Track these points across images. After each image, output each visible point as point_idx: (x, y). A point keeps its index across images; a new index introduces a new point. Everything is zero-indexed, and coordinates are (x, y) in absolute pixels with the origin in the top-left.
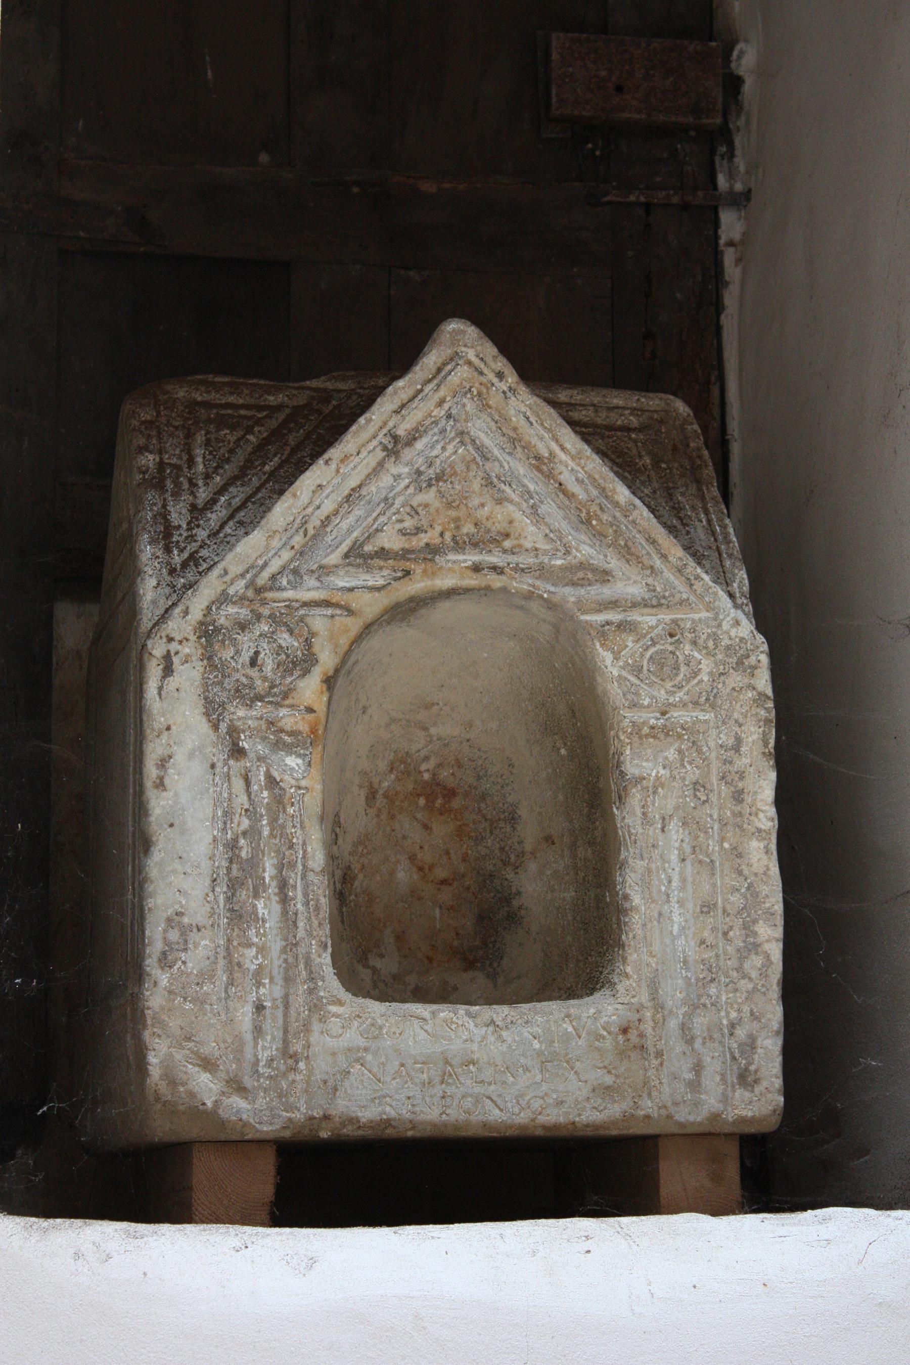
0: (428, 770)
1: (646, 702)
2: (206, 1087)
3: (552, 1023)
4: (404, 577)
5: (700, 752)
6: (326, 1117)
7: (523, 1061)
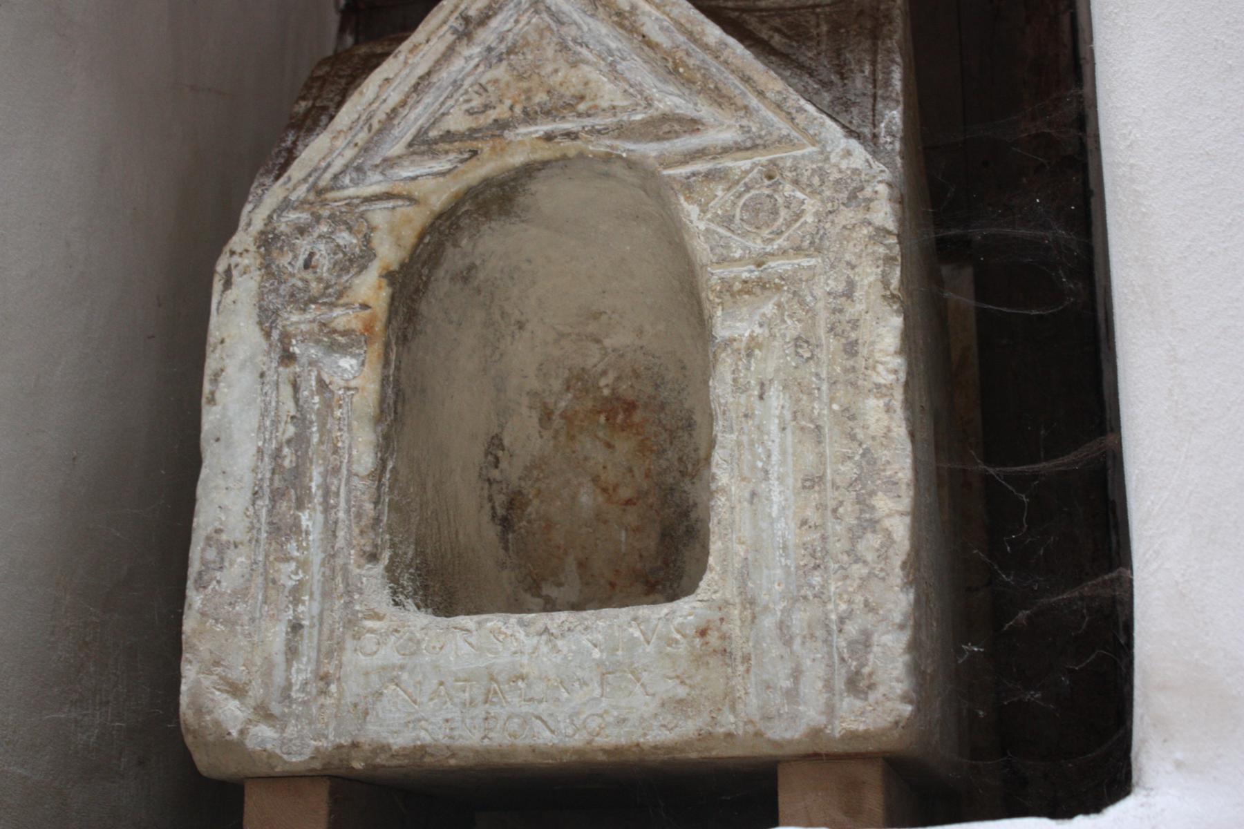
0: (607, 385)
1: (737, 255)
2: (231, 713)
3: (616, 627)
4: (471, 158)
5: (802, 303)
6: (355, 745)
7: (579, 673)
